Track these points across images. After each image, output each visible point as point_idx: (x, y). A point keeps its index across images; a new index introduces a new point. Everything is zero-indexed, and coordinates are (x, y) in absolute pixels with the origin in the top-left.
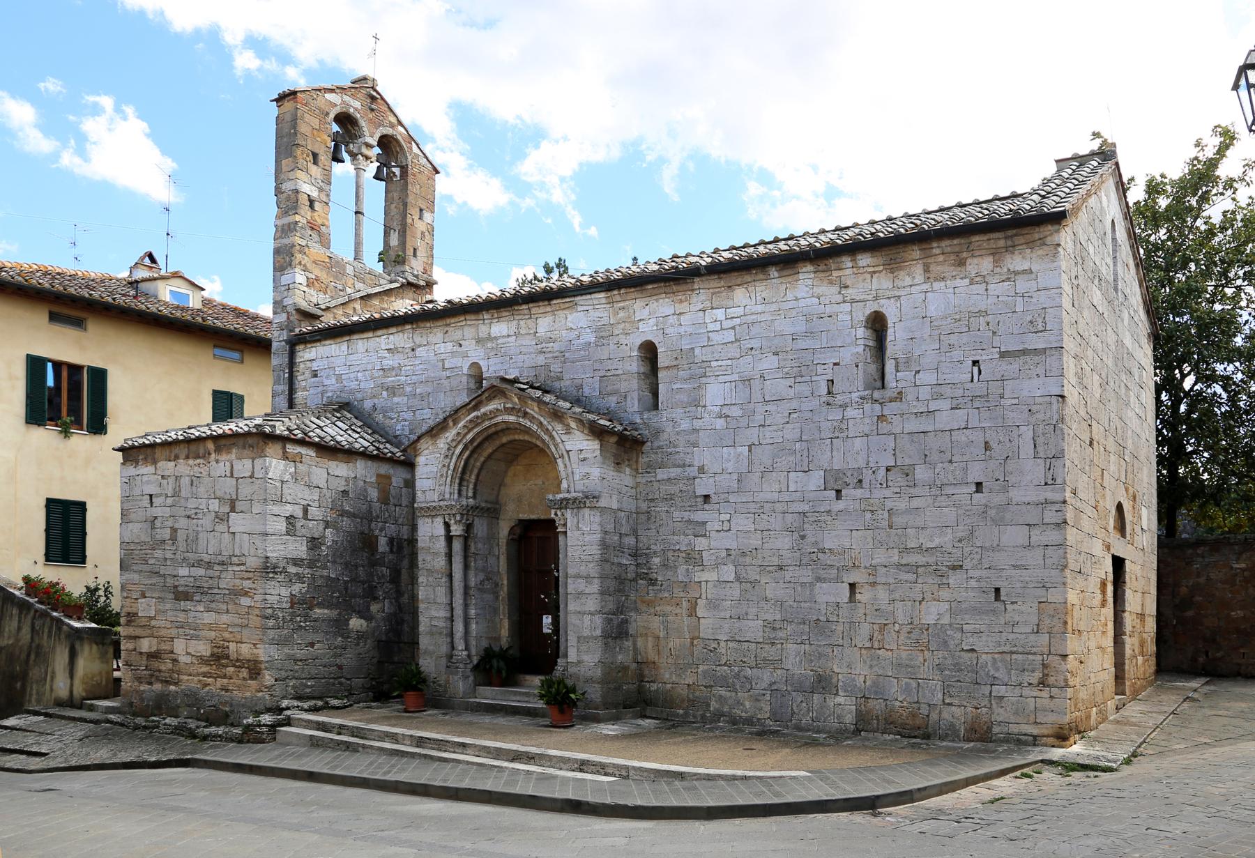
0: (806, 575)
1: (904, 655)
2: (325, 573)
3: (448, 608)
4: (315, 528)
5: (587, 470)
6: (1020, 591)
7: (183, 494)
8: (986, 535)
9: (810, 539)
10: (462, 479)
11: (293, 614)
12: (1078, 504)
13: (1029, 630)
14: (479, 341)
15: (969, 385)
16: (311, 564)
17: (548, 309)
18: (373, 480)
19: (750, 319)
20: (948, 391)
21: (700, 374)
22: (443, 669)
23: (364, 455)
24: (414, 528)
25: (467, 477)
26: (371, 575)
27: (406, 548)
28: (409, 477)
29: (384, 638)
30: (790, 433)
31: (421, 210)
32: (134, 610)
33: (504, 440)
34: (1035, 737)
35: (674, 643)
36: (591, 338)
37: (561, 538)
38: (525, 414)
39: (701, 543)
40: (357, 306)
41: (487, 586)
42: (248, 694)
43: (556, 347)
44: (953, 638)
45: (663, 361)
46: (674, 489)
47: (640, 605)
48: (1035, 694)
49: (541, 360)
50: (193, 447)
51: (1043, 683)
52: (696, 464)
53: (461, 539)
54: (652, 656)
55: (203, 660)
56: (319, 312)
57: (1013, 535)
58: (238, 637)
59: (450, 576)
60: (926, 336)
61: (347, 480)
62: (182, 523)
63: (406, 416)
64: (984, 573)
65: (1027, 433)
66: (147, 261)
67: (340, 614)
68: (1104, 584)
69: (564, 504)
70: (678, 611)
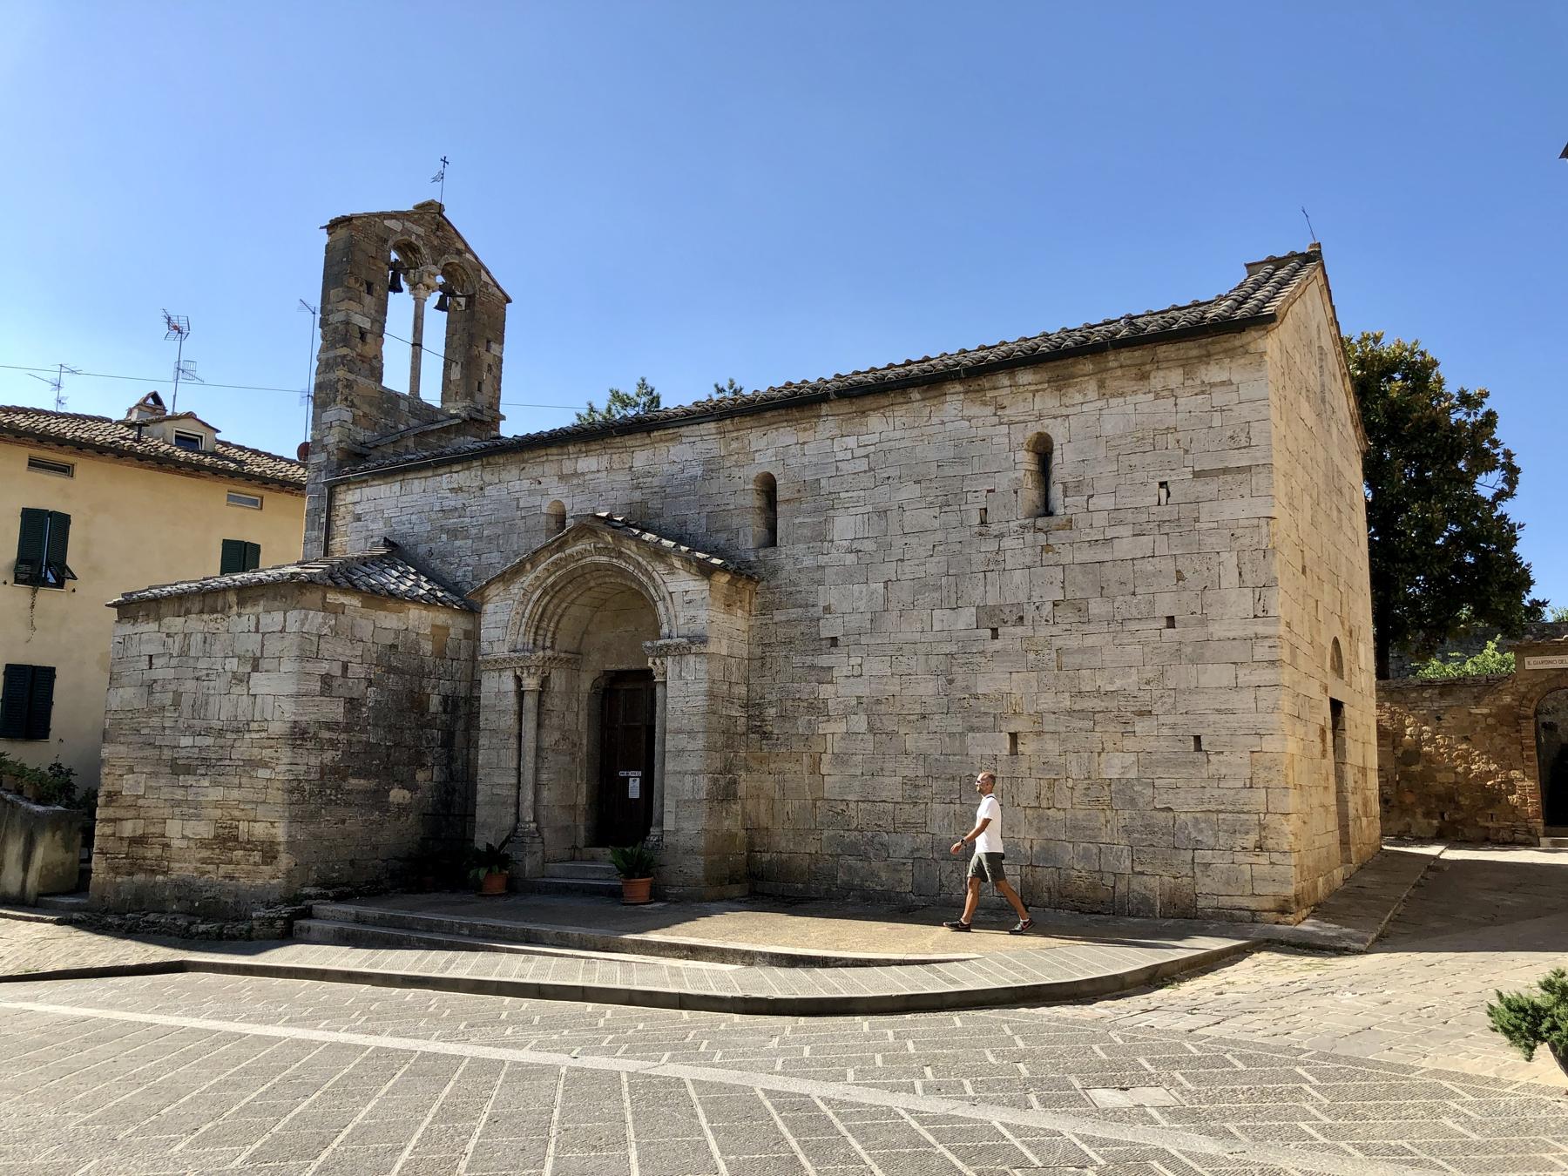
0: (956, 724)
1: (1080, 814)
2: (364, 737)
5: (693, 613)
6: (1227, 739)
7: (192, 653)
8: (1180, 675)
9: (960, 683)
11: (322, 788)
12: (1293, 640)
13: (1240, 784)
14: (562, 477)
15: (1155, 509)
16: (348, 728)
17: (648, 441)
18: (428, 631)
19: (886, 446)
20: (1130, 517)
21: (826, 508)
24: (475, 684)
26: (420, 738)
28: (470, 627)
30: (933, 567)
32: (117, 788)
34: (1253, 912)
35: (791, 806)
36: (698, 471)
37: (659, 689)
38: (620, 555)
39: (826, 691)
42: (259, 882)
43: (656, 481)
44: (1142, 794)
45: (781, 494)
46: (796, 632)
48: (1250, 860)
49: (637, 496)
50: (209, 601)
51: (1260, 847)
52: (822, 604)
53: (535, 696)
54: (765, 820)
55: (203, 844)
56: (365, 451)
57: (1216, 675)
58: (252, 815)
60: (1101, 457)
61: (397, 632)
64: (1180, 719)
65: (1230, 559)
66: (151, 401)
68: (1323, 731)
70: (798, 767)
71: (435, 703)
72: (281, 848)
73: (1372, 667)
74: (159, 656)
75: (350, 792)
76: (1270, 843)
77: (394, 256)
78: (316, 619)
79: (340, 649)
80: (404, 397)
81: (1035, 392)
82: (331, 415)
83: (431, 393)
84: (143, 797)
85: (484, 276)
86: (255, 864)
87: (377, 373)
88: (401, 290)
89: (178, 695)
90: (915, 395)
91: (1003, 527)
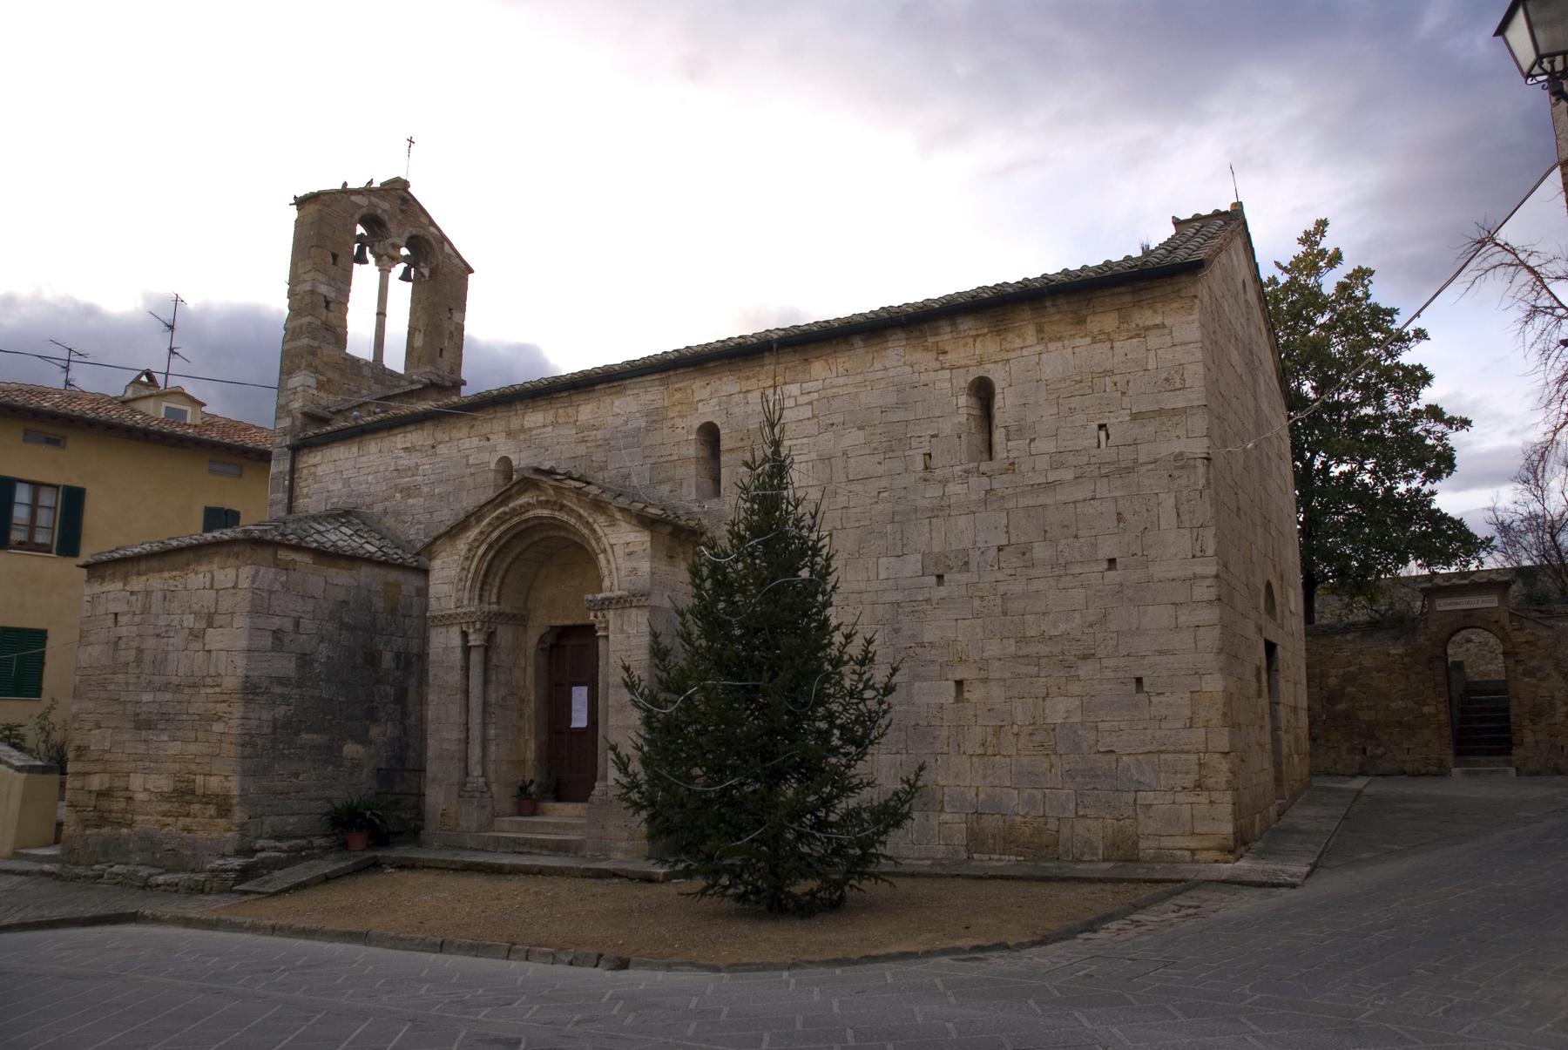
2: (316, 693)
5: (634, 564)
7: (154, 610)
10: (483, 583)
14: (510, 434)
15: (1096, 452)
19: (830, 392)
23: (369, 560)
24: (425, 641)
25: (490, 580)
27: (414, 663)
33: (536, 538)
34: (1193, 851)
37: (601, 643)
38: (562, 507)
42: (215, 835)
43: (600, 434)
45: (725, 443)
49: (582, 450)
51: (1199, 786)
53: (481, 650)
55: (163, 797)
56: (329, 415)
59: (467, 693)
62: (151, 643)
66: (144, 379)
69: (606, 604)
71: (387, 660)
72: (235, 801)
73: (1301, 611)
74: (124, 614)
75: (302, 747)
76: (1210, 782)
77: (360, 230)
78: (268, 574)
80: (367, 363)
81: (975, 337)
82: (296, 381)
83: (395, 359)
84: (109, 751)
85: (447, 248)
86: (211, 817)
87: (340, 338)
88: (366, 262)
89: (140, 651)
90: (858, 342)
91: (947, 471)
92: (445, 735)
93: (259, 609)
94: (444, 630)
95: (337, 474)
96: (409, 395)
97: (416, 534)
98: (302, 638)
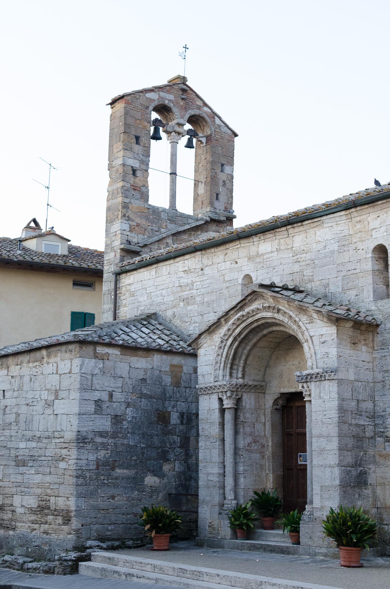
2: (125, 442)
3: (221, 466)
4: (118, 408)
5: (327, 350)
7: (25, 388)
10: (232, 365)
11: (98, 474)
16: (114, 435)
17: (301, 228)
18: (168, 369)
22: (216, 516)
23: (159, 350)
25: (236, 362)
27: (191, 419)
29: (173, 492)
31: (222, 165)
33: (265, 332)
36: (335, 247)
37: (307, 405)
40: (170, 241)
41: (254, 447)
42: (61, 536)
43: (308, 256)
47: (377, 458)
49: (296, 268)
53: (232, 411)
55: (32, 511)
56: (138, 249)
59: (223, 440)
61: (145, 370)
62: (23, 409)
63: (196, 320)
66: (33, 225)
67: (137, 473)
69: (308, 379)
71: (174, 418)
72: (72, 514)
78: (91, 364)
79: (107, 383)
80: (164, 210)
86: (59, 525)
87: (145, 197)
88: (160, 138)
92: (210, 470)
93: (86, 387)
94: (207, 397)
95: (148, 290)
96: (197, 228)
97: (193, 329)
98: (115, 405)
